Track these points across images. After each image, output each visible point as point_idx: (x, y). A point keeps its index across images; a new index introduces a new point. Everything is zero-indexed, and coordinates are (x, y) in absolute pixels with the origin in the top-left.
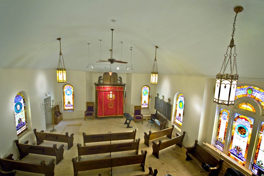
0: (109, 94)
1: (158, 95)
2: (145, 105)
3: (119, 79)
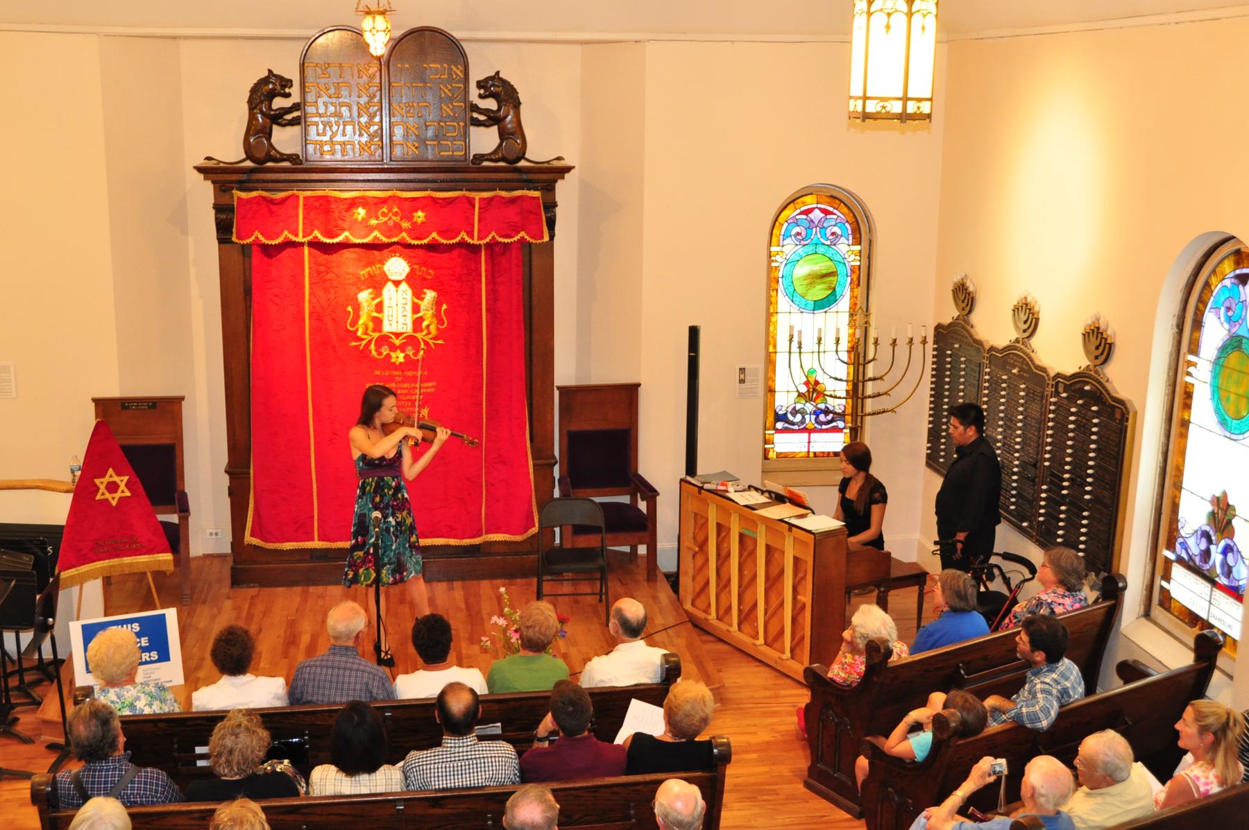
0: (377, 283)
1: (964, 296)
2: (810, 421)
3: (491, 104)
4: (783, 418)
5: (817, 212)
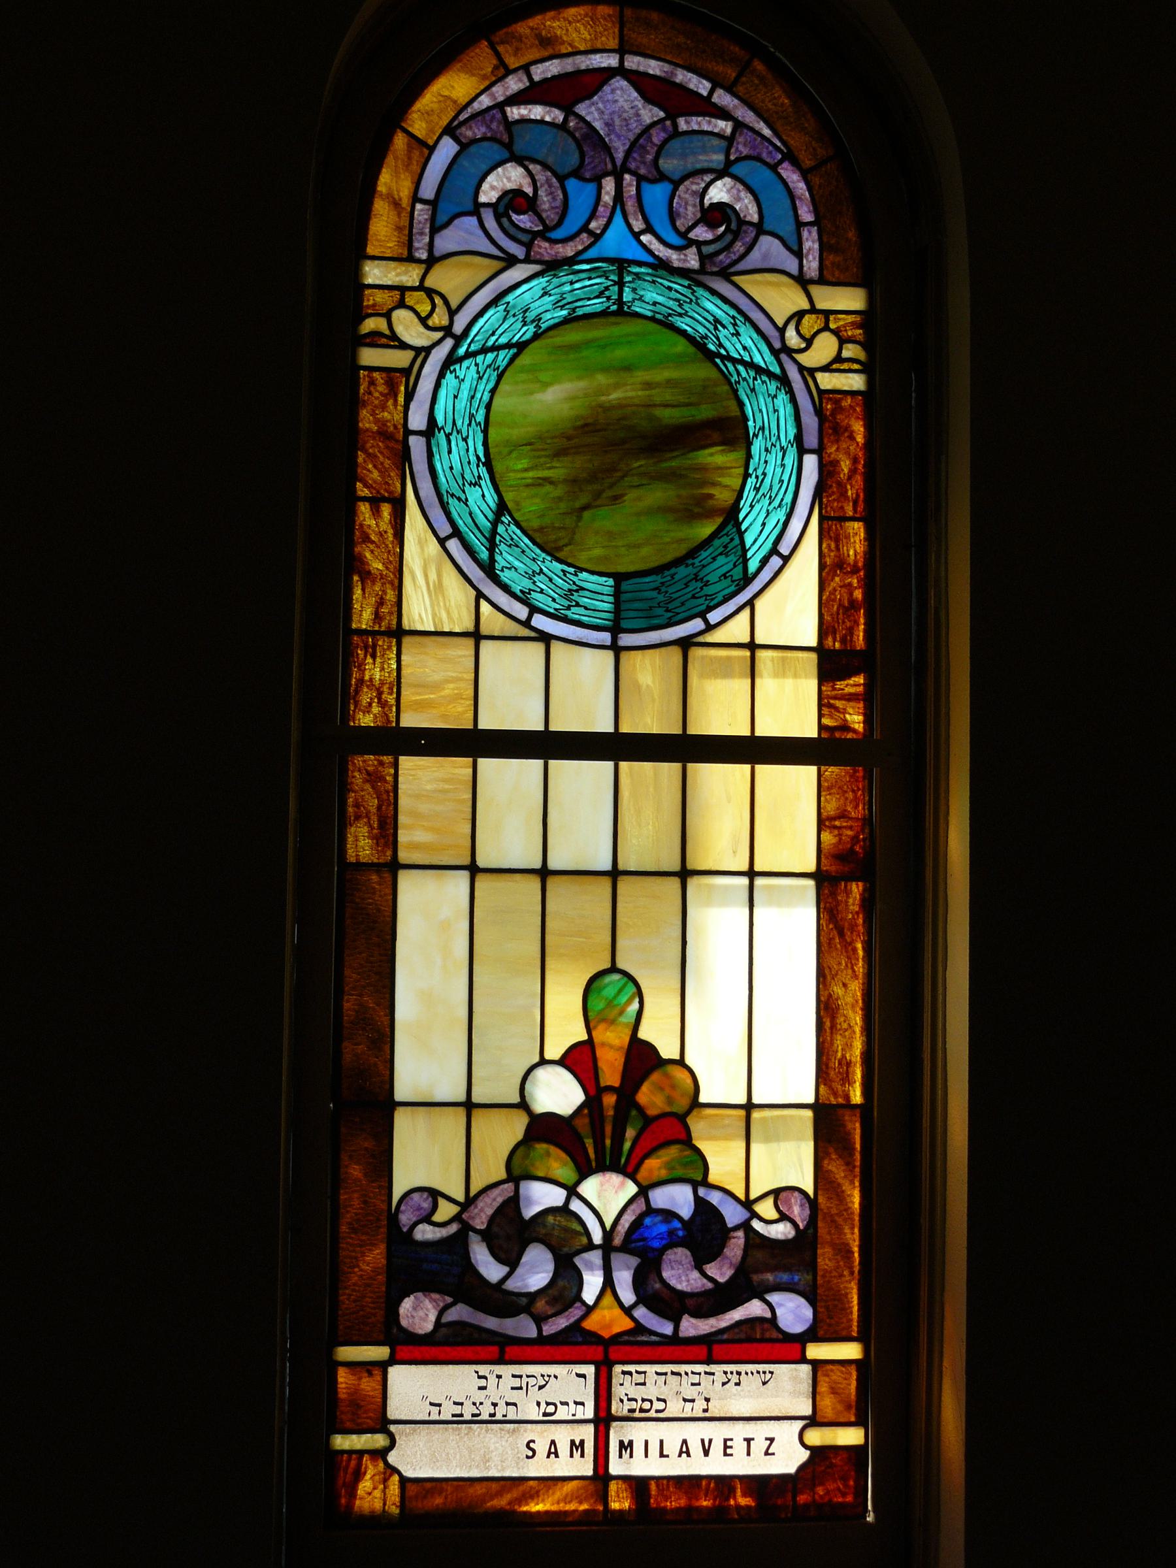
4: (445, 1269)
5: (622, 94)
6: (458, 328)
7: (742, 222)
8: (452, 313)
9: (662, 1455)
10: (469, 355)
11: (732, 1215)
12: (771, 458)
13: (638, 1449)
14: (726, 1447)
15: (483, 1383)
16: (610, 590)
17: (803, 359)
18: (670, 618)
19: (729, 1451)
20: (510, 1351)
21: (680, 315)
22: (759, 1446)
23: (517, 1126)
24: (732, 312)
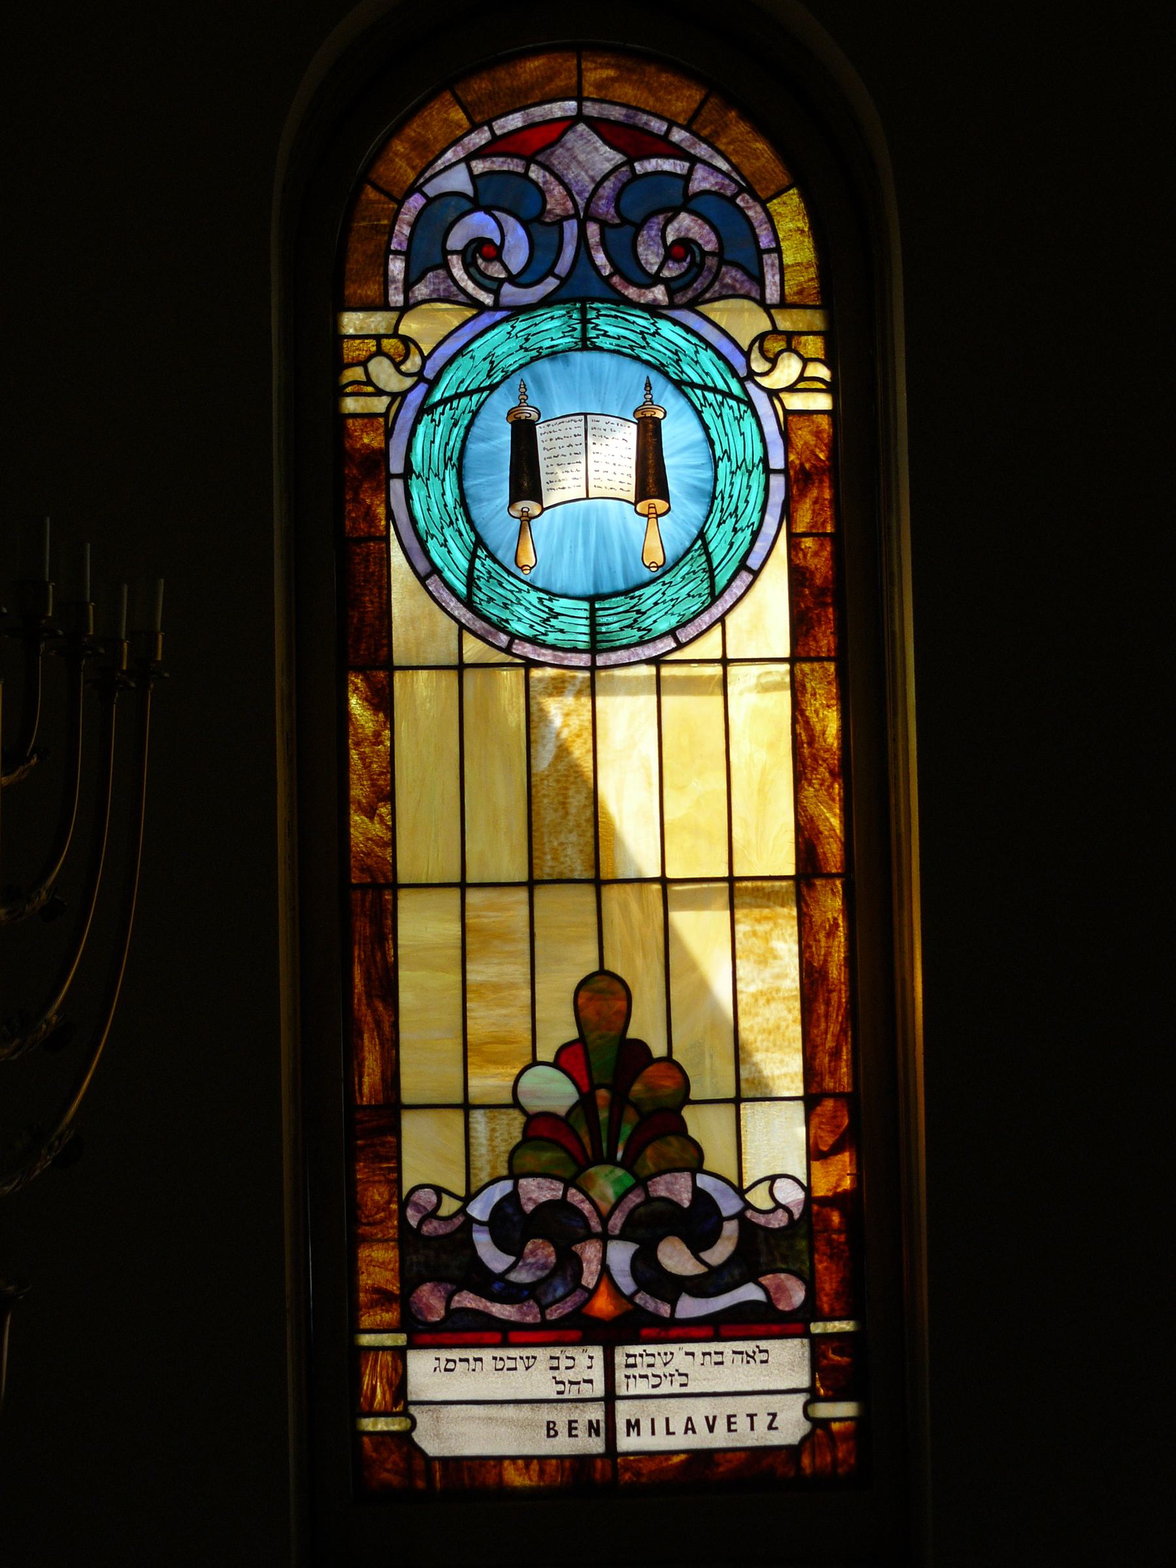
6: (429, 374)
7: (704, 254)
8: (425, 359)
9: (668, 1433)
10: (444, 401)
11: (729, 1205)
12: (737, 480)
13: (645, 1425)
14: (729, 1423)
15: (555, 1363)
16: (586, 614)
17: (765, 382)
18: (641, 637)
19: (574, 1432)
20: (514, 1336)
21: (644, 348)
22: (762, 1421)
23: (512, 1127)
24: (694, 340)
